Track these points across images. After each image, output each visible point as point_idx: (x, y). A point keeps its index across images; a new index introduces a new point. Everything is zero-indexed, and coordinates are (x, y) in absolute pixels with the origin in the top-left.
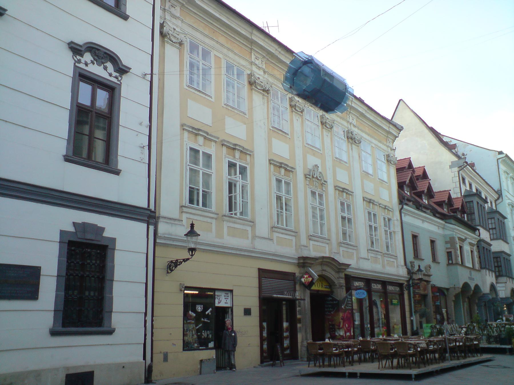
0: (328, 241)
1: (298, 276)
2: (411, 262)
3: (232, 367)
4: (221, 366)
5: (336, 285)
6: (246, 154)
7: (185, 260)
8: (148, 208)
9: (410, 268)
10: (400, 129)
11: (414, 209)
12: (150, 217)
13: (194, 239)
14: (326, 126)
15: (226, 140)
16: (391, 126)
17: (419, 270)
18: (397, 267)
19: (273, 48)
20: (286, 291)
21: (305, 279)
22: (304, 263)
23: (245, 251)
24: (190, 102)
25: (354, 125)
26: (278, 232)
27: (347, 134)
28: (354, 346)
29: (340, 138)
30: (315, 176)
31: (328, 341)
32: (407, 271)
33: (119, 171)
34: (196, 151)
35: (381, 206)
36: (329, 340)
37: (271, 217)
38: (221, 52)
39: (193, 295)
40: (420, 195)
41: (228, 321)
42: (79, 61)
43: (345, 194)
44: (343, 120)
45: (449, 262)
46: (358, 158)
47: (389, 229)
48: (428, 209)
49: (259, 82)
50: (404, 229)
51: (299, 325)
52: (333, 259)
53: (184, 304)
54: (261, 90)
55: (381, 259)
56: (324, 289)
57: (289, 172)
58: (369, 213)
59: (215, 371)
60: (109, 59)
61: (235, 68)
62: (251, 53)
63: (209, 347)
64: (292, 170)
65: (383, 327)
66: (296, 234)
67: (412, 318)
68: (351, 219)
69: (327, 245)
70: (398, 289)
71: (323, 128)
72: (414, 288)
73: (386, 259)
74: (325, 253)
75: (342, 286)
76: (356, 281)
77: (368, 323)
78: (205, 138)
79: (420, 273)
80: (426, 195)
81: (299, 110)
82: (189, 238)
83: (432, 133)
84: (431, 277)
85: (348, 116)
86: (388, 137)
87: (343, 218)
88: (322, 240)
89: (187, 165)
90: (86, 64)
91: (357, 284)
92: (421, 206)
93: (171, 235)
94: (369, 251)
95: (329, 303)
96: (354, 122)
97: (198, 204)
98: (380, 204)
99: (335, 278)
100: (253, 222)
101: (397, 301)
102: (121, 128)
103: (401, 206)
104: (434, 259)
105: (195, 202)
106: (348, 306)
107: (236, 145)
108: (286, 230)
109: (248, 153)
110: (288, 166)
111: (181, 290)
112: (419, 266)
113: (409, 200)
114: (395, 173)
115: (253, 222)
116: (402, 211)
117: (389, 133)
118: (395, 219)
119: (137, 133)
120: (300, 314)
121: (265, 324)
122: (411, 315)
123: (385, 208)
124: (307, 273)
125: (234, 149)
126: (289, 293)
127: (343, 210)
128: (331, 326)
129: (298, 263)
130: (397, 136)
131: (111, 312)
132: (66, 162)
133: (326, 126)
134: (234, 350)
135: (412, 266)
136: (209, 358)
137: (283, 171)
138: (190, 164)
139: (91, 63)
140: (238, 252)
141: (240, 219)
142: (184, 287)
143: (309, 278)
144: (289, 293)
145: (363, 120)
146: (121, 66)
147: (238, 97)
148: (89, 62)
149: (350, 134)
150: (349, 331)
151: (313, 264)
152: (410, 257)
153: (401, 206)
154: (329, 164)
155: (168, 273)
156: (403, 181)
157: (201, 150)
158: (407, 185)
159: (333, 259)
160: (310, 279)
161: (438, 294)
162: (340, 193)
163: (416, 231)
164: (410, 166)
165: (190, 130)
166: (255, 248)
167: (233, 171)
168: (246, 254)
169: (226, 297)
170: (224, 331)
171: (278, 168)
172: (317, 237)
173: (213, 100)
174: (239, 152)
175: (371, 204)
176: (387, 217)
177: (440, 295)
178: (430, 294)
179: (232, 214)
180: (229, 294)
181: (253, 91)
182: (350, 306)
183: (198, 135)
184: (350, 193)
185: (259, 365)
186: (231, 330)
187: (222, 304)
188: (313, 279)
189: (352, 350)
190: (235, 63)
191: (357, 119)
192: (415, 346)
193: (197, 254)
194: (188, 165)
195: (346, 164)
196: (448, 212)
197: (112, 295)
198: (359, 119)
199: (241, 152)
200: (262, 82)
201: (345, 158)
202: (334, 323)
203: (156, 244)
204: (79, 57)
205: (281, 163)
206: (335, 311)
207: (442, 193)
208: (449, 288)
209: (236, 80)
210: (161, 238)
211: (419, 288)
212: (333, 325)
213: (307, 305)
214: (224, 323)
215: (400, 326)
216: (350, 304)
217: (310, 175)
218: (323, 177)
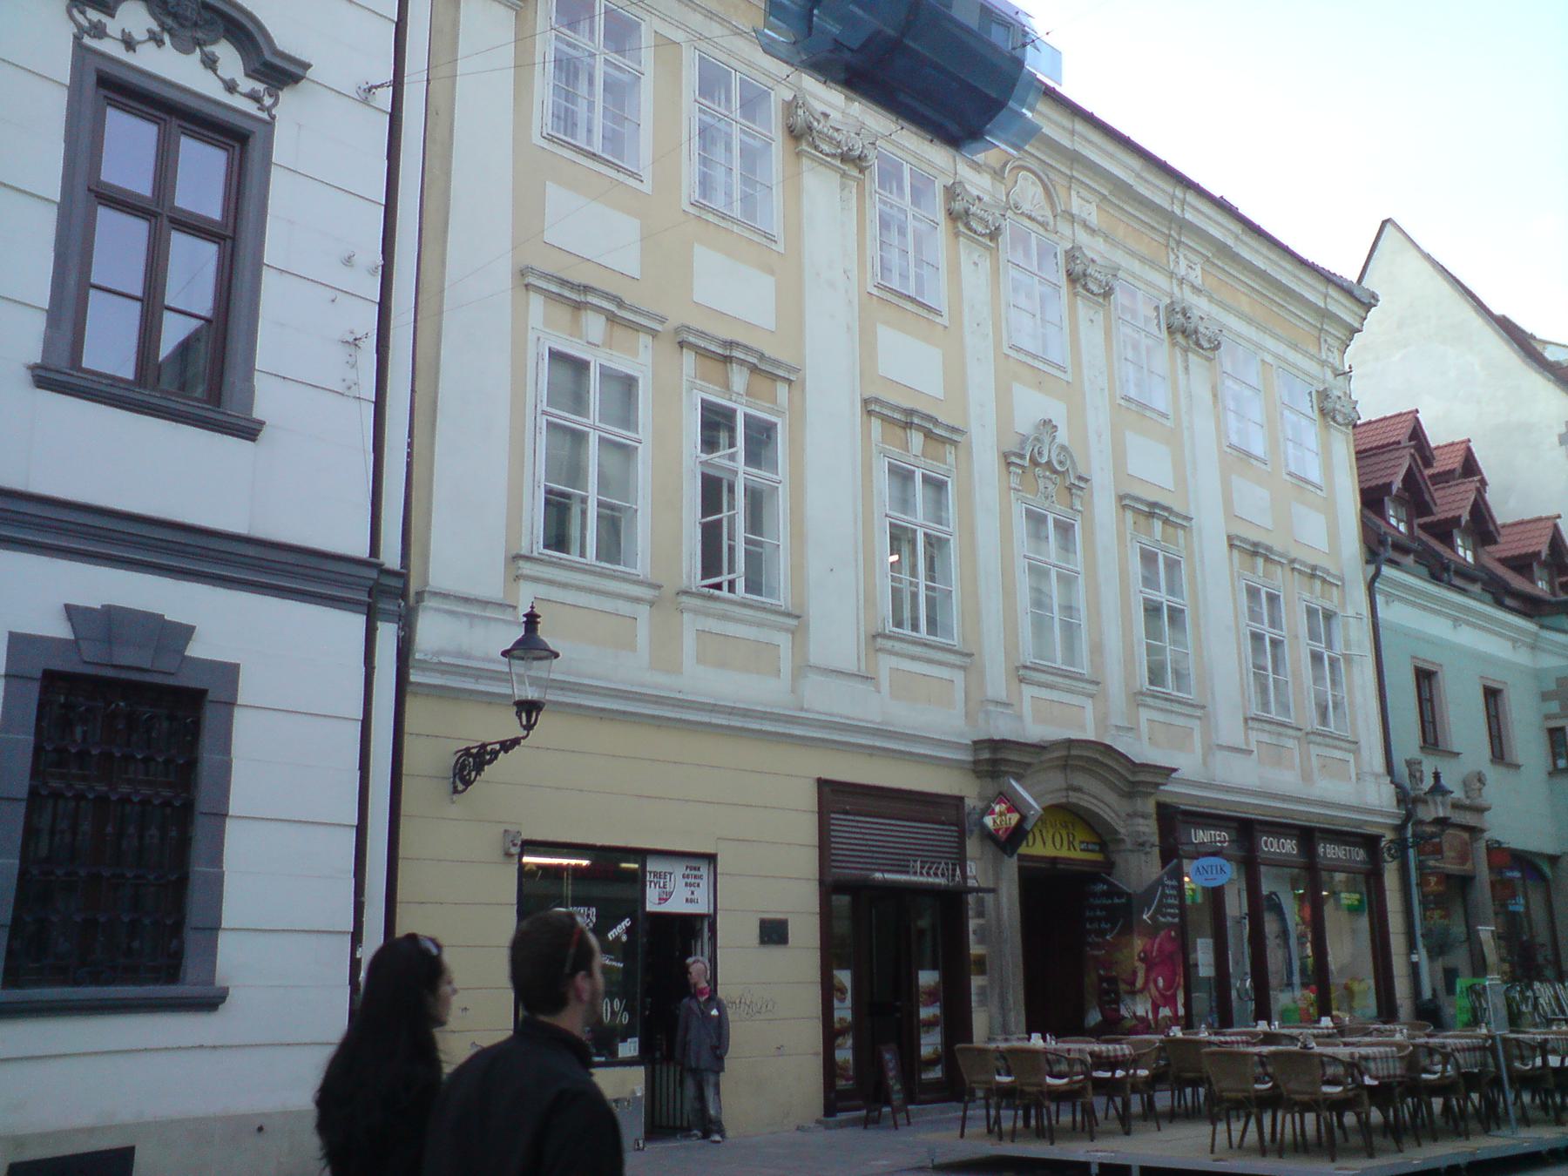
0: (1095, 688)
1: (974, 808)
2: (1409, 763)
3: (709, 1127)
4: (678, 1123)
5: (1122, 841)
6: (775, 378)
7: (507, 745)
8: (373, 560)
9: (1407, 783)
10: (1366, 301)
11: (1421, 578)
12: (377, 591)
13: (539, 669)
14: (1085, 287)
15: (694, 324)
16: (1332, 292)
17: (1438, 789)
18: (1358, 779)
19: (1121, 167)
20: (920, 859)
21: (995, 816)
22: (994, 762)
23: (762, 718)
24: (556, 196)
25: (1193, 286)
26: (896, 654)
27: (1168, 318)
28: (1135, 1062)
29: (1138, 330)
30: (1044, 460)
31: (1180, 1035)
32: (1397, 793)
33: (258, 428)
34: (579, 367)
35: (1297, 566)
36: (1044, 1039)
37: (870, 600)
38: (681, 26)
39: (577, 868)
40: (1444, 531)
41: (697, 966)
42: (99, 31)
43: (1158, 525)
44: (1150, 266)
45: (1555, 764)
46: (1208, 396)
47: (1330, 645)
48: (1472, 579)
49: (825, 130)
50: (1383, 648)
51: (976, 982)
52: (1109, 750)
53: (518, 903)
54: (834, 156)
55: (1297, 752)
56: (1077, 854)
57: (944, 443)
58: (1253, 593)
59: (641, 1142)
60: (221, 30)
61: (906, 169)
62: (1070, 188)
63: (620, 1056)
64: (955, 437)
65: (1305, 985)
66: (968, 660)
67: (1415, 958)
68: (1183, 611)
69: (1090, 701)
70: (1360, 855)
71: (1076, 294)
72: (1420, 852)
73: (1314, 750)
74: (1083, 728)
75: (1143, 844)
76: (1199, 826)
77: (1246, 974)
78: (612, 318)
79: (1439, 799)
80: (1466, 532)
81: (980, 229)
82: (518, 667)
83: (1497, 327)
84: (1486, 813)
85: (1172, 257)
86: (1321, 330)
87: (1152, 610)
88: (1068, 681)
89: (539, 411)
90: (129, 44)
91: (1201, 836)
92: (1446, 568)
93: (469, 658)
94: (1251, 723)
95: (1098, 902)
96: (1196, 276)
97: (915, 627)
98: (1293, 561)
99: (1118, 815)
100: (798, 617)
101: (1357, 896)
102: (268, 277)
103: (1371, 569)
104: (1499, 752)
105: (575, 546)
106: (1164, 915)
107: (730, 344)
108: (925, 645)
109: (781, 373)
110: (936, 422)
111: (508, 855)
112: (1437, 776)
113: (1399, 547)
114: (1350, 455)
115: (798, 617)
116: (1376, 584)
117: (1325, 314)
118: (1350, 612)
119: (331, 294)
120: (981, 941)
121: (844, 977)
122: (1412, 947)
123: (1313, 574)
124: (1002, 797)
125: (727, 360)
126: (930, 868)
127: (1150, 581)
128: (1105, 985)
129: (976, 762)
130: (1357, 325)
131: (214, 928)
132: (39, 390)
133: (1085, 287)
134: (718, 1066)
135: (1412, 775)
136: (621, 1096)
137: (917, 439)
138: (549, 409)
139: (150, 39)
140: (737, 722)
141: (744, 605)
142: (519, 843)
143: (1008, 815)
144: (930, 868)
145: (1227, 268)
146: (268, 56)
147: (919, 262)
148: (139, 34)
149: (1179, 316)
150: (1171, 1001)
151: (1029, 765)
152: (1408, 741)
153: (1371, 569)
154: (1098, 418)
155: (456, 791)
156: (1381, 482)
157: (597, 360)
158: (1396, 496)
159: (1109, 748)
160: (1014, 818)
161: (1517, 874)
162: (1142, 519)
163: (1430, 657)
164: (1417, 434)
165: (554, 288)
166: (805, 706)
167: (723, 437)
168: (768, 727)
169: (689, 881)
170: (686, 1000)
171: (899, 431)
172: (1052, 674)
173: (646, 187)
174: (746, 371)
175: (1260, 561)
176: (1318, 603)
177: (1523, 878)
178: (1484, 874)
179: (718, 586)
180: (704, 870)
181: (805, 161)
182: (1173, 916)
183: (586, 309)
184: (1179, 521)
185: (818, 1122)
186: (707, 996)
187: (676, 906)
188: (1023, 819)
189: (1127, 1075)
190: (733, 63)
191: (1206, 268)
192: (1355, 1067)
193: (543, 720)
194: (544, 413)
195: (1164, 421)
196: (1554, 593)
197: (222, 867)
198: (1214, 264)
199: (754, 369)
200: (837, 130)
201: (1160, 401)
202: (1114, 973)
203: (409, 689)
204: (94, 15)
205: (910, 412)
206: (1115, 931)
207: (1529, 527)
208: (1559, 854)
209: (738, 119)
210: (426, 666)
211: (1438, 851)
212: (1113, 981)
213: (1005, 912)
214: (685, 970)
215: (1371, 982)
216: (1171, 906)
217: (1022, 457)
218: (1073, 462)
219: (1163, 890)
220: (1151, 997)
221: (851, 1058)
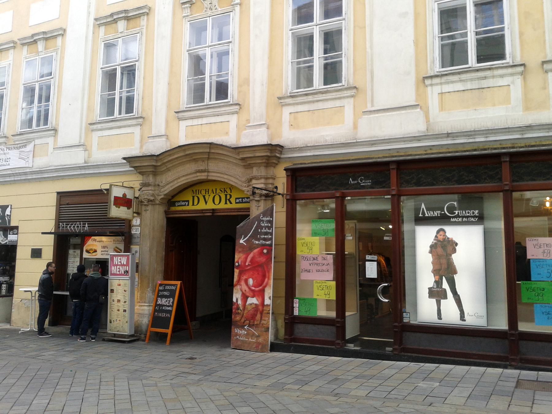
57: (140, 17)
219: (259, 224)
220: (242, 291)
221: (180, 282)
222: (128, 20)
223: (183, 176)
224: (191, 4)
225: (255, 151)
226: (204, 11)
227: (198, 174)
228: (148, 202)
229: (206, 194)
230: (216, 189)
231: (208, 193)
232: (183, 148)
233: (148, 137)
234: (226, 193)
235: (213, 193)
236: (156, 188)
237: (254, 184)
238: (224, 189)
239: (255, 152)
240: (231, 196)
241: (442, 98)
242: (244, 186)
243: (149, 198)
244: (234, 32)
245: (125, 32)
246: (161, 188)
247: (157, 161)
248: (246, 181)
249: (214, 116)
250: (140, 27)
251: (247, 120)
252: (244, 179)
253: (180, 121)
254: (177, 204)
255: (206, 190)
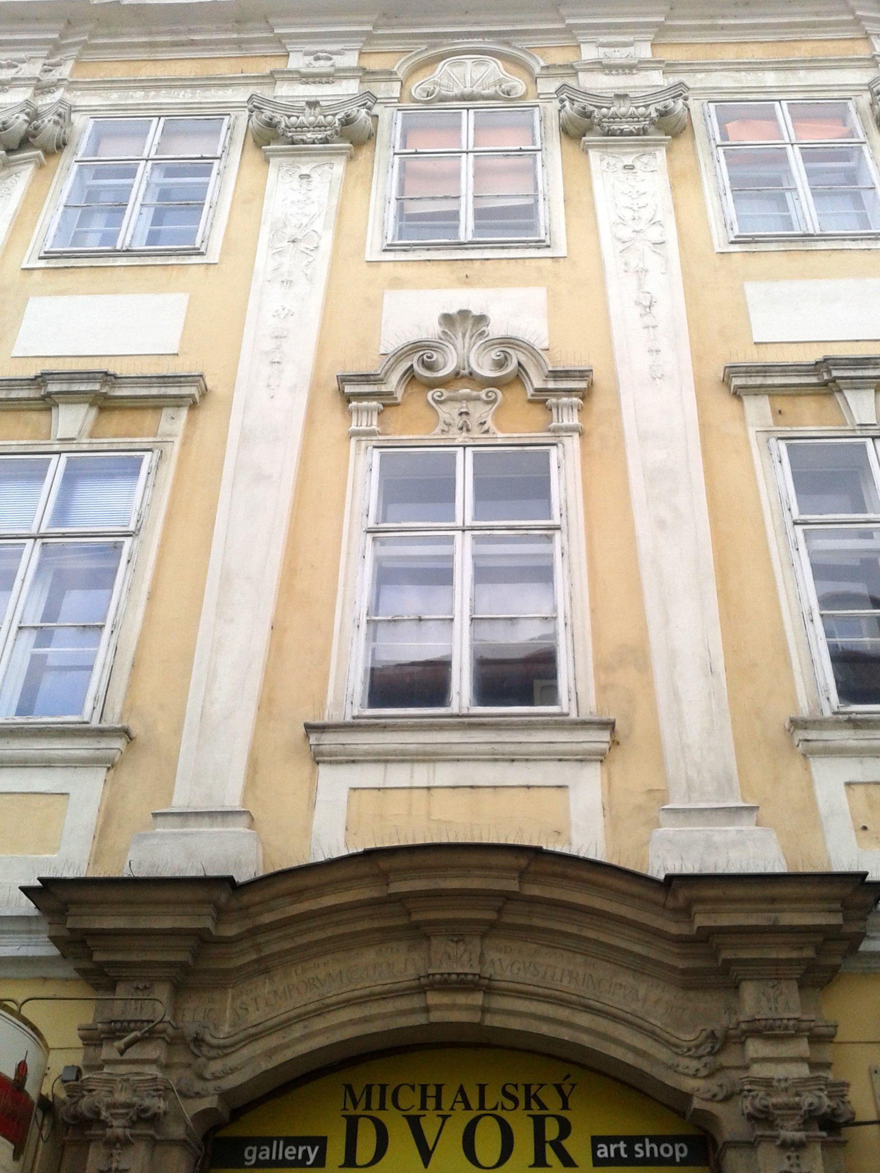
57: (158, 408)
222: (102, 409)
223: (349, 1003)
224: (384, 405)
225: (773, 900)
226: (438, 430)
227: (433, 998)
228: (133, 1124)
229: (423, 1107)
230: (482, 1088)
231: (438, 1107)
232: (385, 864)
233: (155, 815)
234: (536, 1110)
235: (468, 1107)
236: (181, 1057)
237: (755, 1060)
238: (528, 1087)
239: (778, 906)
240: (565, 1128)
241: (320, 1030)
242: (691, 1072)
243: (147, 1102)
244: (566, 501)
245: (85, 440)
246: (210, 1059)
247: (221, 913)
248: (697, 1047)
249: (495, 759)
250: (155, 435)
251: (651, 791)
252: (687, 1037)
253: (323, 769)
254: (251, 1155)
255: (424, 1088)
